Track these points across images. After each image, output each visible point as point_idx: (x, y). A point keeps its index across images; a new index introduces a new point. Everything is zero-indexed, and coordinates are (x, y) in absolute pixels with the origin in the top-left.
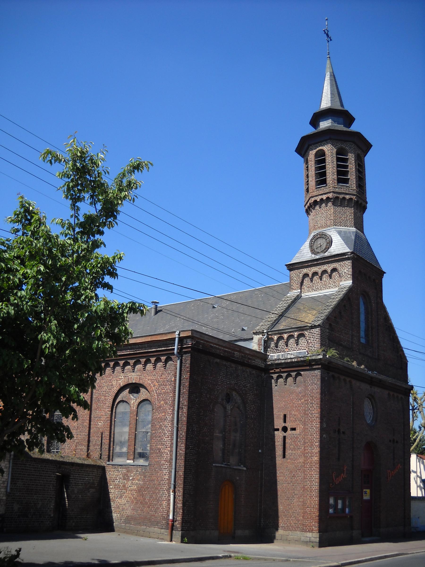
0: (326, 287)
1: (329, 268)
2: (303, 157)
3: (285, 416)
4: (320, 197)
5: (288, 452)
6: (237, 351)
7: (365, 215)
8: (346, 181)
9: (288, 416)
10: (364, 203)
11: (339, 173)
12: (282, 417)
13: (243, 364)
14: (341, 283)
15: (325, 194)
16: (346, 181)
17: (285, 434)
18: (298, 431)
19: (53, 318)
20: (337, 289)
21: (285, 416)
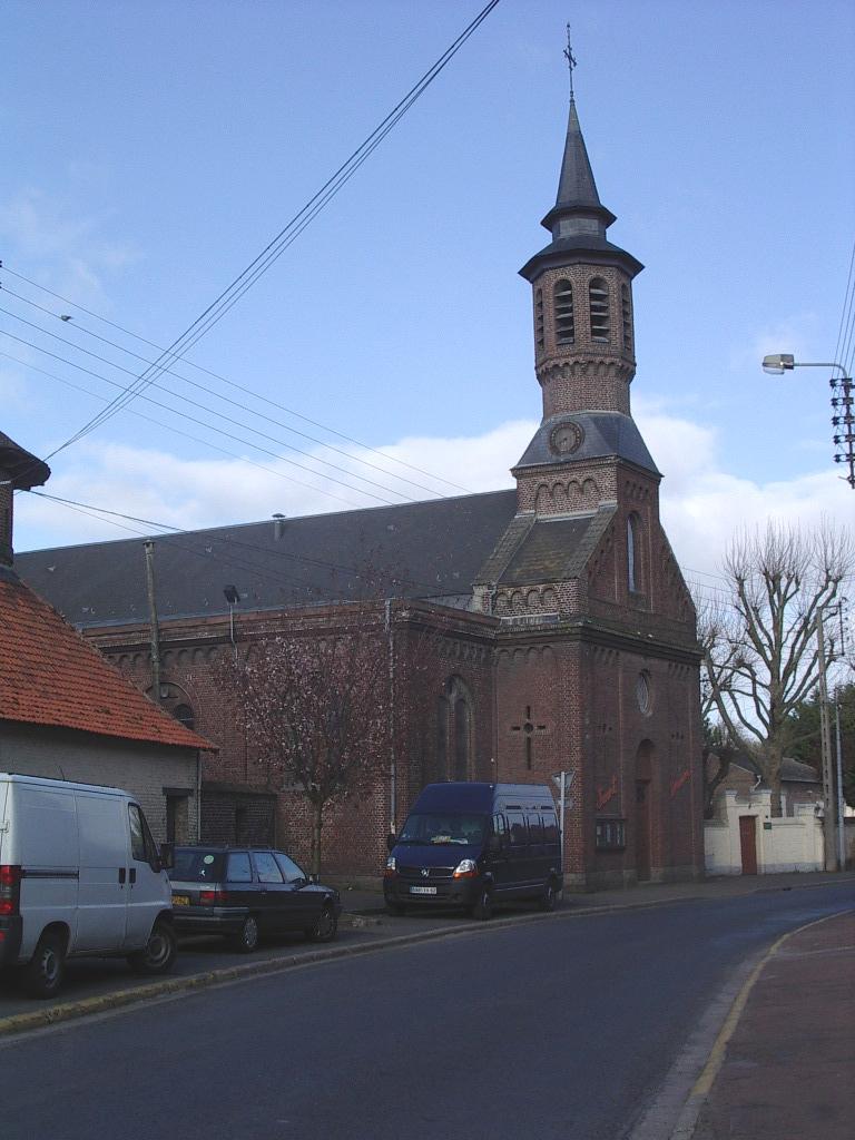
0: (575, 508)
1: (580, 477)
2: (532, 282)
3: (529, 708)
4: (563, 361)
5: (536, 760)
6: (460, 619)
7: (631, 385)
8: (742, 819)
9: (533, 709)
10: (631, 367)
11: (595, 320)
12: (524, 709)
13: (468, 637)
14: (600, 503)
15: (572, 356)
16: (742, 819)
17: (529, 735)
18: (548, 731)
19: (470, 866)
20: (595, 511)
21: (529, 708)
